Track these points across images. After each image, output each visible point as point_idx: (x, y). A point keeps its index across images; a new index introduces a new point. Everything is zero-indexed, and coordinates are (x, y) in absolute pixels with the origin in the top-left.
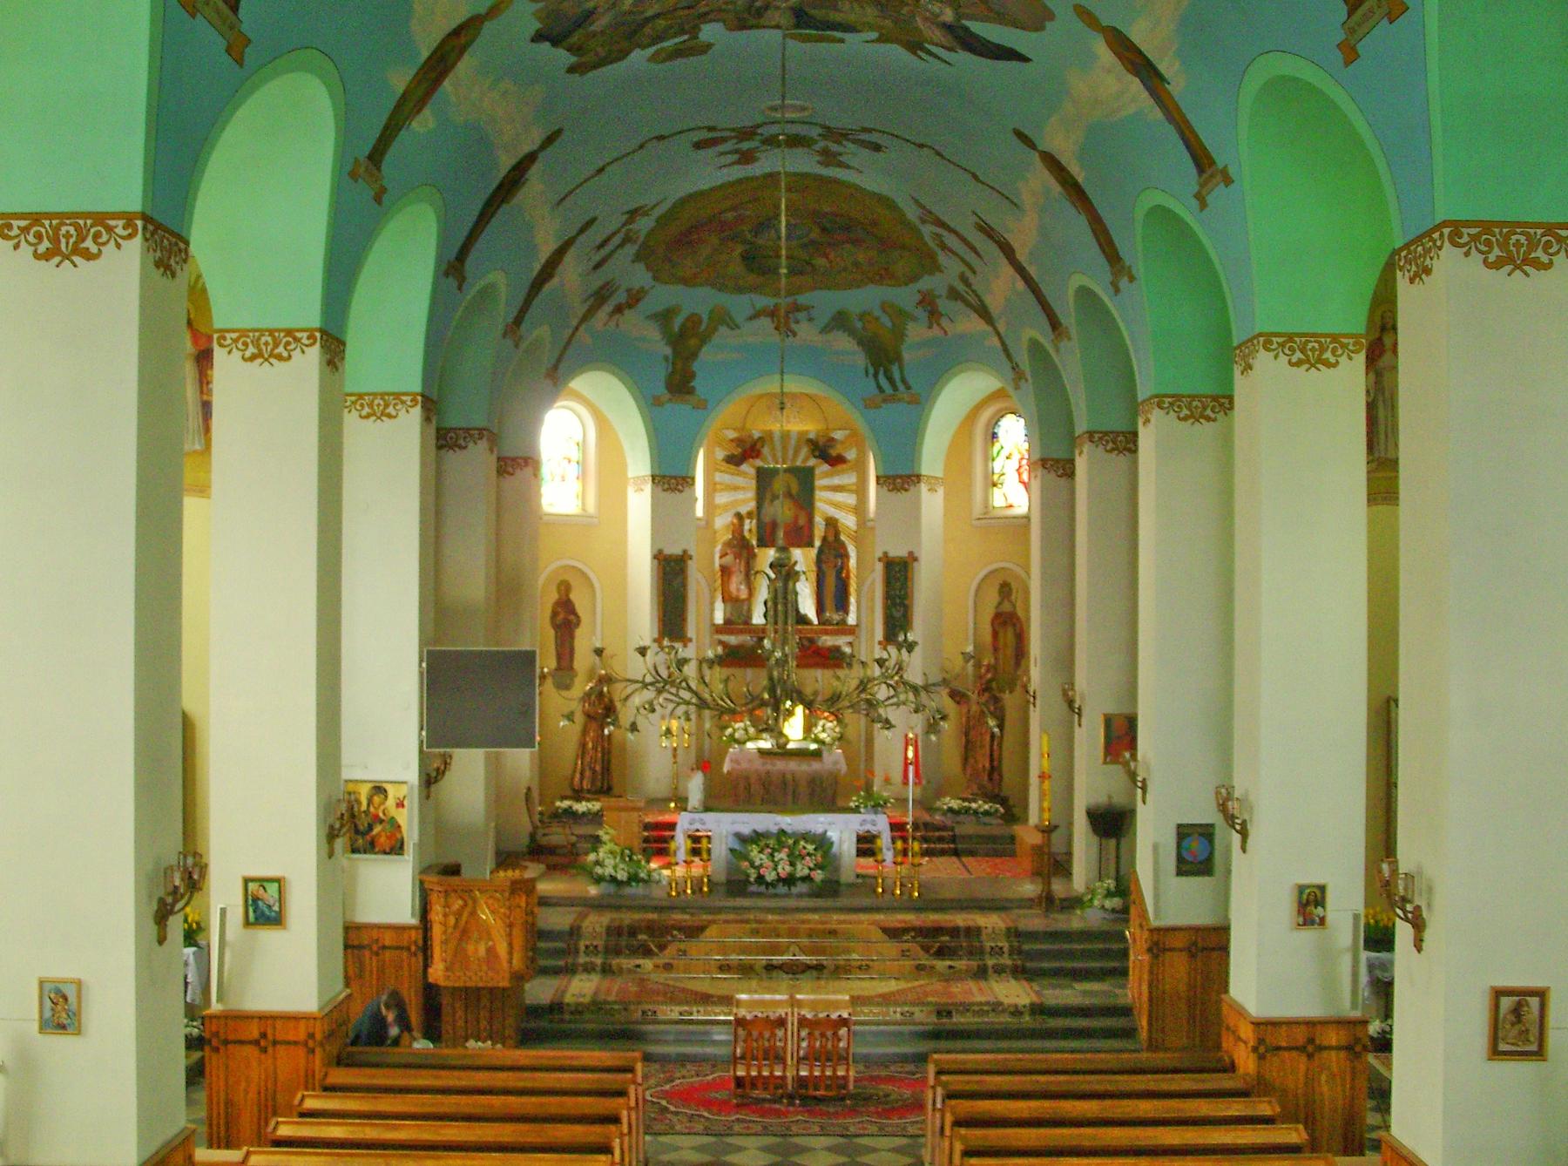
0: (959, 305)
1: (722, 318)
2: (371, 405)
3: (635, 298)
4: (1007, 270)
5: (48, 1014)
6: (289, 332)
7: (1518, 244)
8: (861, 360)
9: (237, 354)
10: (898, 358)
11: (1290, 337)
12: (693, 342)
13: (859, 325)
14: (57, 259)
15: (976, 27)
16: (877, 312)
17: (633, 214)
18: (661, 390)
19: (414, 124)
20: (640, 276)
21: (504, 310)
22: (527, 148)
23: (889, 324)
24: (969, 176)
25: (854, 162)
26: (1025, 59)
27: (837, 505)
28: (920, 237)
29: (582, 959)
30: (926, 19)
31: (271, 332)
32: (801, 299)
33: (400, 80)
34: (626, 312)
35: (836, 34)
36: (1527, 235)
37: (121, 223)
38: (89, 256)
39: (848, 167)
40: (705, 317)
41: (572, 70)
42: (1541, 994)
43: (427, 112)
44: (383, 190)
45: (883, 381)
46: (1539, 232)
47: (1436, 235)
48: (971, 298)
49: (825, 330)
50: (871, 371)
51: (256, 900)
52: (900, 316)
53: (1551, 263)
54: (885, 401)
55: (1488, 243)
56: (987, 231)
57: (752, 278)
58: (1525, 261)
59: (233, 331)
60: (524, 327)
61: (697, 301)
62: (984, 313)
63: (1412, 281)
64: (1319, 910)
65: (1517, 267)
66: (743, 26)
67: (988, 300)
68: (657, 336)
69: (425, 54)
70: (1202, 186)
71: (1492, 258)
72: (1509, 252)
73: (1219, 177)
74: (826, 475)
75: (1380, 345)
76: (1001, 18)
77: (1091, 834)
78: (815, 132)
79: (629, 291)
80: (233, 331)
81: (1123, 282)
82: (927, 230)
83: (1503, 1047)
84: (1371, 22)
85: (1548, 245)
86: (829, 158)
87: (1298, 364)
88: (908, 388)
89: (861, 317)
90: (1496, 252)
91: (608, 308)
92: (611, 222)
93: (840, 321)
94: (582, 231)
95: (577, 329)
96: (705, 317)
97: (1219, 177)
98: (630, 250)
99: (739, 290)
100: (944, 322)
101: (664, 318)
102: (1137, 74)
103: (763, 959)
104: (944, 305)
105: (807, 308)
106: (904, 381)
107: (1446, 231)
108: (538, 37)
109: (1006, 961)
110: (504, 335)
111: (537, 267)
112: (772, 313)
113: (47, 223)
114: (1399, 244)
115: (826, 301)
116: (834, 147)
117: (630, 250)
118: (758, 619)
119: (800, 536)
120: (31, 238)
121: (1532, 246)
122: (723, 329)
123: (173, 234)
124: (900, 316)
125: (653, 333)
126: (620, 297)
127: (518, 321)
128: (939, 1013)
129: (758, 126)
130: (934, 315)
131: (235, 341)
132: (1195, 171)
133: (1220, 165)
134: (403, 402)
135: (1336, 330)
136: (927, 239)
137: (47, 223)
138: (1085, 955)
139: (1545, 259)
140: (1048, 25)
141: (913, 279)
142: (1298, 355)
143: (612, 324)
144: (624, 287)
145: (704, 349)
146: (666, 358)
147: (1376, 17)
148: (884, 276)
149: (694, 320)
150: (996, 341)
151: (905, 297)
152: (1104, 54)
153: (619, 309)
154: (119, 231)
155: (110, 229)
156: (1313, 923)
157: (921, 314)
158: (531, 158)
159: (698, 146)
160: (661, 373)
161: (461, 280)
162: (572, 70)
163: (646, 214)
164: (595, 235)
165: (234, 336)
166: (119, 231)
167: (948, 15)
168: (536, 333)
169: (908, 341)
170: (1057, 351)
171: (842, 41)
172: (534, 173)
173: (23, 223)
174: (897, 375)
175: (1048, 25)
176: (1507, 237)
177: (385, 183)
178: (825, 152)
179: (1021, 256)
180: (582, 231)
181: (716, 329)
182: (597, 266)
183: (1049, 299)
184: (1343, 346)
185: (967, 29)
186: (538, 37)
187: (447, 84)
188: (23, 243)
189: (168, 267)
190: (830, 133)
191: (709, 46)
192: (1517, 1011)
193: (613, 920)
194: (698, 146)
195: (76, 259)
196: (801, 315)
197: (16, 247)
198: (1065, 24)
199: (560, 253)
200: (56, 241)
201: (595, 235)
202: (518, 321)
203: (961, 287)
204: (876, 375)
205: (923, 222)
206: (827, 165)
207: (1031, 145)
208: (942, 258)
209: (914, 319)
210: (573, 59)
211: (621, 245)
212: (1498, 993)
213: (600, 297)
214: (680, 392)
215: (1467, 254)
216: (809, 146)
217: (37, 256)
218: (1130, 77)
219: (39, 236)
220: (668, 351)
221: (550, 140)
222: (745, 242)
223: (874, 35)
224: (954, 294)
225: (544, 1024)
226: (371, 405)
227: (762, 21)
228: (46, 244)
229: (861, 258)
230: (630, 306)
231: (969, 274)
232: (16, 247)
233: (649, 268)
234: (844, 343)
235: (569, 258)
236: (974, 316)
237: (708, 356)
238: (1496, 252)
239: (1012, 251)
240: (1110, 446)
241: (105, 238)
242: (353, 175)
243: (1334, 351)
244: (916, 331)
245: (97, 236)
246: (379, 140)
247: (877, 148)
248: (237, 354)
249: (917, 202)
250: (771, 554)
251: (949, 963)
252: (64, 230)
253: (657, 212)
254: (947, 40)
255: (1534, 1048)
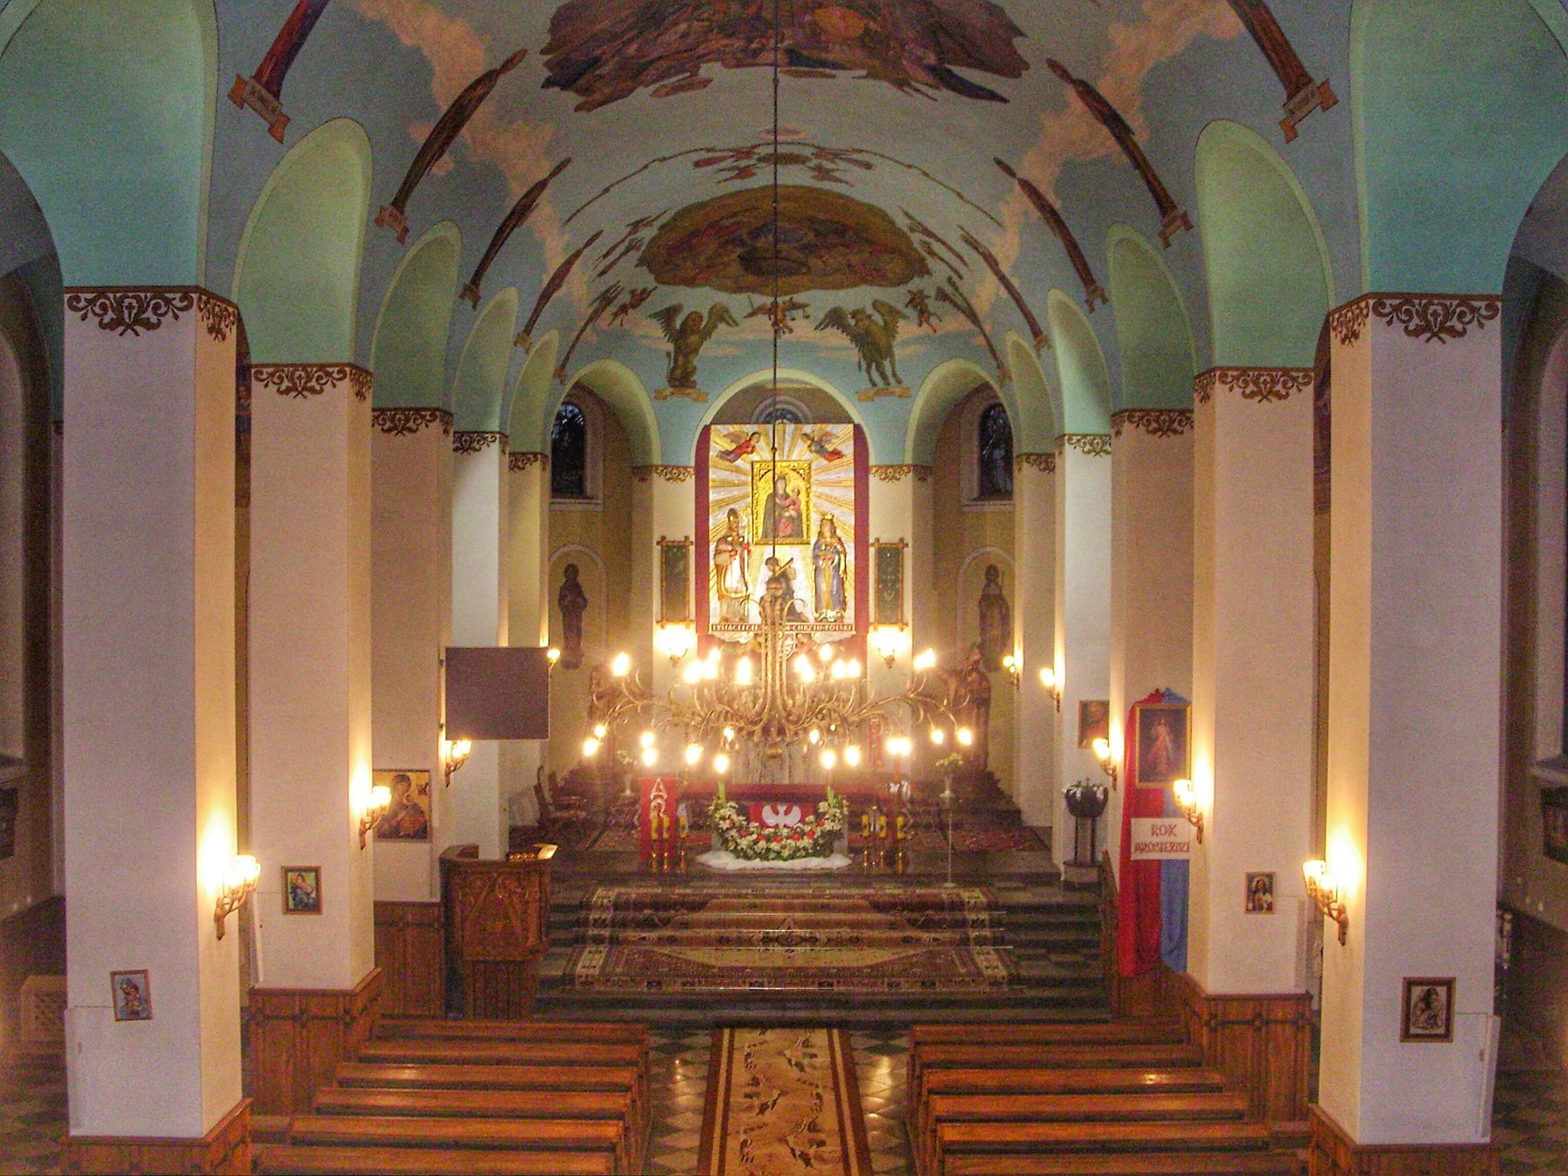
0: (947, 305)
1: (721, 315)
2: (392, 419)
3: (639, 298)
4: (991, 278)
5: (121, 1003)
6: (322, 367)
7: (1435, 314)
8: (854, 354)
9: (273, 388)
10: (889, 353)
11: (1244, 371)
12: (694, 338)
13: (852, 322)
14: (121, 329)
15: (957, 70)
16: (870, 311)
17: (636, 226)
18: (662, 382)
19: (434, 170)
20: (646, 279)
21: (513, 327)
22: (541, 177)
23: (881, 323)
24: (954, 196)
25: (847, 177)
26: (1004, 101)
27: (829, 499)
28: (909, 243)
29: (592, 932)
30: (913, 62)
31: (305, 367)
32: (800, 298)
33: (421, 134)
34: (630, 311)
35: (828, 71)
36: (1445, 307)
37: (178, 296)
38: (150, 326)
39: (840, 181)
40: (705, 313)
41: (578, 108)
42: (1449, 984)
43: (446, 157)
44: (406, 230)
45: (876, 376)
46: (1455, 303)
47: (1363, 304)
48: (960, 301)
49: (821, 326)
50: (864, 366)
51: (295, 888)
52: (892, 314)
53: (1465, 330)
54: (877, 393)
55: (1408, 312)
56: (974, 244)
57: (750, 279)
58: (1443, 329)
59: (268, 366)
60: (534, 332)
61: (697, 299)
62: (972, 316)
63: (1343, 341)
64: (1267, 897)
65: (1435, 335)
66: (739, 65)
67: (975, 303)
68: (660, 333)
69: (444, 108)
70: (1166, 226)
71: (1412, 327)
72: (1427, 321)
73: (1178, 222)
74: (823, 470)
75: (1322, 379)
76: (981, 65)
77: (1068, 814)
78: (808, 152)
79: (633, 292)
80: (268, 366)
81: (1098, 302)
82: (916, 238)
83: (1413, 1031)
84: (1307, 108)
85: (1461, 315)
86: (822, 173)
87: (1252, 395)
88: (899, 382)
89: (854, 314)
90: (1416, 321)
91: (613, 308)
92: (615, 231)
93: (835, 319)
94: (588, 244)
95: (583, 331)
96: (705, 313)
97: (1178, 222)
98: (635, 255)
99: (739, 289)
100: (933, 320)
101: (667, 315)
102: (1105, 122)
103: (759, 933)
104: (932, 304)
105: (803, 306)
106: (894, 375)
107: (1371, 302)
108: (548, 83)
109: (987, 933)
110: (515, 344)
111: (546, 279)
112: (772, 310)
113: (111, 296)
114: (1332, 306)
115: (821, 300)
116: (828, 165)
117: (635, 255)
118: (754, 616)
119: (797, 534)
120: (97, 310)
121: (1448, 315)
122: (722, 326)
123: (223, 300)
124: (892, 314)
125: (656, 330)
126: (625, 298)
127: (528, 330)
128: (923, 984)
129: (755, 147)
130: (924, 314)
131: (272, 375)
132: (1157, 211)
133: (1181, 210)
134: (423, 417)
135: (1288, 365)
136: (916, 245)
137: (111, 296)
138: (1063, 926)
139: (1459, 327)
140: (1024, 73)
141: (903, 280)
142: (1251, 388)
143: (617, 322)
144: (629, 288)
145: (705, 344)
146: (668, 355)
147: (1311, 105)
148: (873, 276)
149: (695, 317)
150: (980, 340)
151: (895, 296)
152: (1077, 104)
153: (623, 309)
154: (177, 303)
155: (168, 302)
156: (1261, 908)
157: (911, 313)
158: (542, 185)
159: (697, 164)
160: (664, 366)
161: (476, 300)
162: (578, 108)
163: (650, 224)
164: (600, 247)
165: (271, 370)
166: (177, 303)
167: (931, 59)
168: (546, 337)
169: (899, 338)
170: (1039, 356)
171: (833, 77)
172: (544, 198)
173: (90, 296)
174: (889, 372)
175: (1024, 73)
176: (1426, 308)
177: (409, 224)
178: (819, 169)
179: (1005, 268)
180: (588, 244)
181: (715, 326)
182: (602, 273)
183: (1030, 307)
184: (1294, 379)
185: (949, 71)
186: (548, 83)
187: (464, 131)
188: (90, 314)
189: (219, 331)
190: (821, 152)
191: (710, 81)
192: (1427, 999)
193: (619, 895)
194: (697, 164)
195: (138, 328)
196: (798, 313)
197: (84, 318)
198: (1038, 75)
199: (568, 264)
200: (118, 310)
201: (600, 247)
202: (528, 330)
203: (949, 290)
204: (869, 366)
205: (912, 230)
206: (823, 179)
207: (1012, 174)
208: (931, 263)
209: (905, 317)
210: (580, 99)
211: (627, 251)
212: (1410, 984)
213: (606, 299)
214: (682, 385)
215: (1390, 323)
216: (804, 162)
217: (102, 326)
218: (1099, 125)
219: (104, 308)
220: (671, 347)
221: (558, 170)
222: (743, 244)
223: (864, 73)
224: (942, 295)
225: (556, 993)
226: (392, 419)
227: (758, 61)
228: (110, 315)
229: (855, 260)
230: (634, 307)
231: (955, 278)
232: (84, 318)
233: (651, 271)
234: (836, 338)
235: (576, 268)
236: (962, 317)
237: (708, 349)
238: (1416, 321)
239: (996, 263)
240: (1088, 447)
241: (163, 309)
242: (379, 222)
243: (1284, 384)
244: (907, 329)
245: (156, 307)
246: (400, 192)
247: (868, 166)
248: (273, 388)
249: (906, 214)
250: (767, 551)
251: (933, 935)
252: (127, 301)
253: (663, 220)
254: (930, 79)
255: (1442, 1031)
